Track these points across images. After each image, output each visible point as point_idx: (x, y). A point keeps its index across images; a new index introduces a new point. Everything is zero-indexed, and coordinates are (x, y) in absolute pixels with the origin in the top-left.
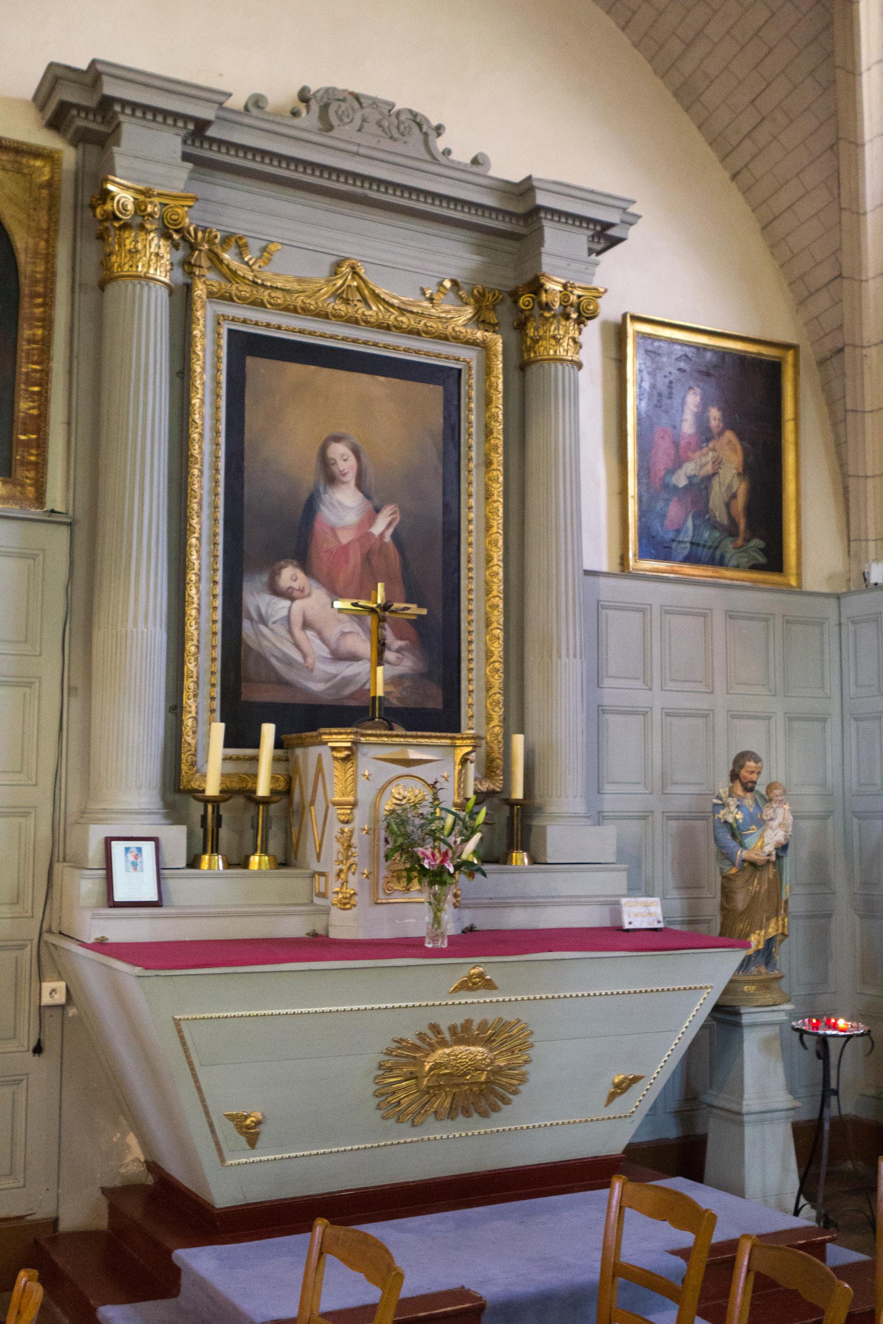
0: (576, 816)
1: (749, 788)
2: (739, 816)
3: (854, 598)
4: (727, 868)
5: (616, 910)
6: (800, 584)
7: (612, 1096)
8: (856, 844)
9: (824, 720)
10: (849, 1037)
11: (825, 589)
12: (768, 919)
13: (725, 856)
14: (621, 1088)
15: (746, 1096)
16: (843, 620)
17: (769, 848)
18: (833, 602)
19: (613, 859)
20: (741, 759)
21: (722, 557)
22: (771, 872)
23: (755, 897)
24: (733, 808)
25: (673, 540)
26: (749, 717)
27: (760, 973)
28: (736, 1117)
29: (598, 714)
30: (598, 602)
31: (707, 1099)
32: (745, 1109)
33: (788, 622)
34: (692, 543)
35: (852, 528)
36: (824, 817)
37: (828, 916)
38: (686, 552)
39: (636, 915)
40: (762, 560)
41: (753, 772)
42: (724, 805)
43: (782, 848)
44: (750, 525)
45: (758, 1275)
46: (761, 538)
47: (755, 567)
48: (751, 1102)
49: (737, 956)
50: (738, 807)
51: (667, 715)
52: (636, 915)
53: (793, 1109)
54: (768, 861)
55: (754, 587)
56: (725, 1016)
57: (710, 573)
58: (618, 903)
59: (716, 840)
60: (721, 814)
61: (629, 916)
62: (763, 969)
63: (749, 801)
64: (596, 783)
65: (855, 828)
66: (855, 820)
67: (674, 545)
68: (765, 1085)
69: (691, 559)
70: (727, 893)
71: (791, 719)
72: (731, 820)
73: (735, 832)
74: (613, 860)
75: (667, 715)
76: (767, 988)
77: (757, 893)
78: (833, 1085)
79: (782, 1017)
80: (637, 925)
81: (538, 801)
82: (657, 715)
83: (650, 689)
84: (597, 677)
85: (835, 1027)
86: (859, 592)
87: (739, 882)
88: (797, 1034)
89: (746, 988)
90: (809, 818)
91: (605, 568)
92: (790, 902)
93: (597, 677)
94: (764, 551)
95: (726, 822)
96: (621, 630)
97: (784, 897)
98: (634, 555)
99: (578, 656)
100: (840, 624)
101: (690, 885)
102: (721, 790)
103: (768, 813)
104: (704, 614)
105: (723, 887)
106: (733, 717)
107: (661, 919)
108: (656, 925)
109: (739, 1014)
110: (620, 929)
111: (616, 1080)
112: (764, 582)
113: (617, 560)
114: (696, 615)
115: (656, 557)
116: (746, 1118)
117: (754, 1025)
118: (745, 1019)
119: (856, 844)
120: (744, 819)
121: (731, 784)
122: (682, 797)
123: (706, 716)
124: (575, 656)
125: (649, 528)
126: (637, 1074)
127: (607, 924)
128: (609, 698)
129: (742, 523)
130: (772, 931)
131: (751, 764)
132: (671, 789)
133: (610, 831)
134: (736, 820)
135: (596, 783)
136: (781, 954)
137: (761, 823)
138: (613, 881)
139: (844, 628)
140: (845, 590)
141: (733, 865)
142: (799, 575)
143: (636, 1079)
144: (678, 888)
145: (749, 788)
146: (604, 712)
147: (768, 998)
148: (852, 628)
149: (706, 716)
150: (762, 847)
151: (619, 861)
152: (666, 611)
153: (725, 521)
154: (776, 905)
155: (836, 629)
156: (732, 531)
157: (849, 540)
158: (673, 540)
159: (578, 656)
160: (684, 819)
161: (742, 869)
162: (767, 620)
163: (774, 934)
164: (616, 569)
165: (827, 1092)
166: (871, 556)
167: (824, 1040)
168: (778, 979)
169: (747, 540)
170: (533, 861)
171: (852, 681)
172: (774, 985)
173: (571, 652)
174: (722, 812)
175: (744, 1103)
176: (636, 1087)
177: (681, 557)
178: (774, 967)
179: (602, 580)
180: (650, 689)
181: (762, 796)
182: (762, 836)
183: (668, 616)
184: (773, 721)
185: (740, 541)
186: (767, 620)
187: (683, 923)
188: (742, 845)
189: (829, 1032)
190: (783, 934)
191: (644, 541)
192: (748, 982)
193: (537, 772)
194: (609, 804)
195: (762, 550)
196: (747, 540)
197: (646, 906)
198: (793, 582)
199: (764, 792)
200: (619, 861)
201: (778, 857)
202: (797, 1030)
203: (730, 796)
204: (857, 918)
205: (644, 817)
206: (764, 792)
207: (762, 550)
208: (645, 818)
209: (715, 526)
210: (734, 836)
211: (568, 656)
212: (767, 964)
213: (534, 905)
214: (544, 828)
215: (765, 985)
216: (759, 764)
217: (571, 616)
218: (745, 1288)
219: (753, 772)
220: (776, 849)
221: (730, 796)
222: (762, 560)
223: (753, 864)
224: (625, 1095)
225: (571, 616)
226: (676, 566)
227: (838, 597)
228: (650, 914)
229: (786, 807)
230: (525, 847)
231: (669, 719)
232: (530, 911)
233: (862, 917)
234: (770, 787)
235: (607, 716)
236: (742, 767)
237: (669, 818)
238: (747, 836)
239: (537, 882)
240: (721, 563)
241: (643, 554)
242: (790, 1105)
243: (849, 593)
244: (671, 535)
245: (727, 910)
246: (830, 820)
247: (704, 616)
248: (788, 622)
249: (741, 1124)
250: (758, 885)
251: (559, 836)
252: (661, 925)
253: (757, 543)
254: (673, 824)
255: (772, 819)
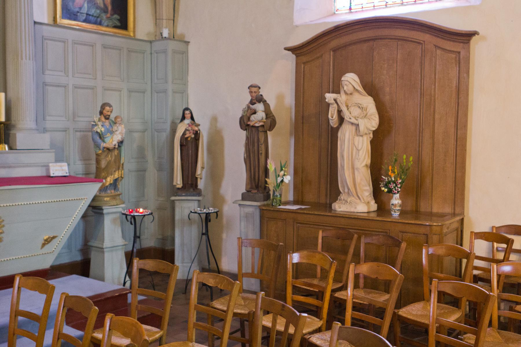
0: (31, 129)
1: (107, 118)
2: (103, 129)
3: (157, 43)
4: (98, 151)
5: (48, 170)
6: (134, 35)
7: (44, 245)
8: (156, 143)
9: (144, 92)
10: (144, 215)
11: (145, 38)
12: (115, 171)
13: (97, 146)
14: (48, 241)
15: (105, 241)
16: (153, 52)
17: (115, 142)
18: (149, 44)
19: (49, 148)
20: (103, 106)
21: (101, 22)
22: (116, 152)
23: (109, 163)
24: (100, 126)
25: (78, 12)
26: (112, 90)
27: (111, 193)
28: (101, 250)
29: (42, 87)
30: (43, 36)
31: (90, 244)
32: (104, 246)
33: (130, 51)
34: (87, 14)
35: (157, 14)
36: (144, 131)
37: (145, 171)
38: (84, 18)
39: (56, 170)
40: (118, 24)
41: (108, 111)
42: (96, 125)
43: (121, 143)
44: (113, 8)
45: (69, 310)
46: (118, 15)
47: (115, 27)
48: (107, 244)
49: (98, 185)
50: (102, 126)
51: (76, 87)
52: (56, 170)
53: (125, 245)
54: (115, 148)
55: (114, 35)
56: (95, 210)
57: (95, 28)
58: (48, 166)
59: (93, 139)
60: (95, 129)
61: (53, 170)
62: (113, 191)
63: (107, 123)
64: (41, 115)
65: (156, 136)
66: (156, 133)
67: (79, 14)
68: (113, 237)
69: (85, 21)
70: (98, 162)
71: (130, 91)
72: (99, 131)
73: (101, 136)
74: (49, 148)
75: (76, 87)
76: (114, 198)
77: (110, 161)
78: (138, 234)
79: (120, 210)
80: (57, 174)
81: (13, 122)
82: (71, 87)
83: (68, 76)
84: (41, 69)
85: (138, 212)
86: (159, 40)
87: (103, 157)
88: (124, 216)
89: (105, 199)
90: (137, 132)
91: (46, 21)
92: (124, 164)
93: (41, 69)
94: (119, 20)
95: (97, 132)
96: (54, 51)
97: (122, 163)
98: (60, 17)
99: (31, 59)
100: (151, 54)
101: (85, 159)
102: (95, 119)
103: (115, 128)
104: (92, 46)
105: (97, 159)
106: (105, 90)
107: (68, 172)
108: (65, 175)
109: (102, 209)
110: (50, 177)
111: (45, 238)
112: (119, 33)
113: (52, 19)
114: (90, 46)
115: (70, 19)
116: (105, 250)
117: (108, 213)
118: (105, 211)
119: (156, 143)
120: (105, 131)
121: (99, 116)
122: (83, 123)
123: (93, 89)
124: (30, 59)
125: (67, 6)
126: (55, 235)
127: (44, 174)
128: (48, 79)
129: (110, 8)
130: (116, 176)
131: (107, 108)
132: (77, 119)
133: (47, 137)
134: (101, 131)
135: (41, 115)
136: (121, 185)
137: (112, 132)
138: (48, 157)
139: (153, 55)
140: (154, 39)
141: (100, 149)
142: (134, 32)
143: (54, 237)
144: (81, 160)
145: (107, 118)
146: (46, 85)
147: (114, 202)
148: (156, 55)
149: (93, 89)
150: (112, 142)
151: (51, 149)
152: (75, 43)
153: (102, 6)
154: (119, 166)
155: (150, 55)
156: (105, 11)
157: (156, 19)
158: (78, 12)
159: (31, 59)
160: (83, 131)
161: (103, 151)
162: (120, 50)
163: (117, 177)
164: (51, 22)
165: (136, 237)
166: (164, 25)
167: (134, 217)
168: (119, 195)
169: (112, 15)
170: (10, 148)
171: (155, 76)
172: (118, 197)
173: (28, 58)
174: (95, 128)
175: (104, 244)
176: (54, 241)
177: (82, 20)
178: (118, 190)
179: (44, 27)
180: (68, 76)
181: (113, 121)
182: (112, 138)
183: (76, 45)
184: (122, 92)
185: (109, 15)
186: (120, 50)
187: (83, 174)
188: (104, 141)
189: (136, 214)
190: (121, 177)
191: (65, 11)
192: (108, 197)
193: (12, 109)
194: (49, 125)
195: (119, 20)
196: (112, 15)
197: (61, 166)
198: (132, 34)
199: (113, 120)
200: (51, 149)
201: (119, 146)
202: (123, 214)
203: (99, 121)
204: (156, 171)
205: (65, 130)
206: (113, 120)
207: (119, 20)
208: (66, 131)
209: (98, 8)
210: (100, 138)
211: (26, 59)
212: (115, 189)
213: (10, 167)
214: (15, 134)
215: (114, 197)
216: (111, 108)
217: (27, 42)
218: (62, 314)
219: (108, 111)
220: (118, 143)
221: (99, 121)
222: (118, 24)
223: (108, 149)
224: (49, 244)
225: (27, 42)
226: (80, 23)
227: (151, 42)
228: (63, 170)
229: (123, 126)
230: (7, 142)
231: (76, 89)
232: (7, 170)
233: (157, 171)
234: (116, 118)
235: (47, 87)
236: (104, 109)
237: (76, 131)
238: (106, 137)
239: (12, 157)
240: (100, 24)
241: (63, 17)
242: (123, 244)
243: (156, 40)
244: (77, 10)
245: (98, 169)
246: (146, 133)
247: (92, 46)
248: (129, 51)
249: (103, 252)
250: (111, 157)
251: (21, 138)
252: (68, 174)
253: (116, 16)
254: (78, 134)
255: (116, 131)
